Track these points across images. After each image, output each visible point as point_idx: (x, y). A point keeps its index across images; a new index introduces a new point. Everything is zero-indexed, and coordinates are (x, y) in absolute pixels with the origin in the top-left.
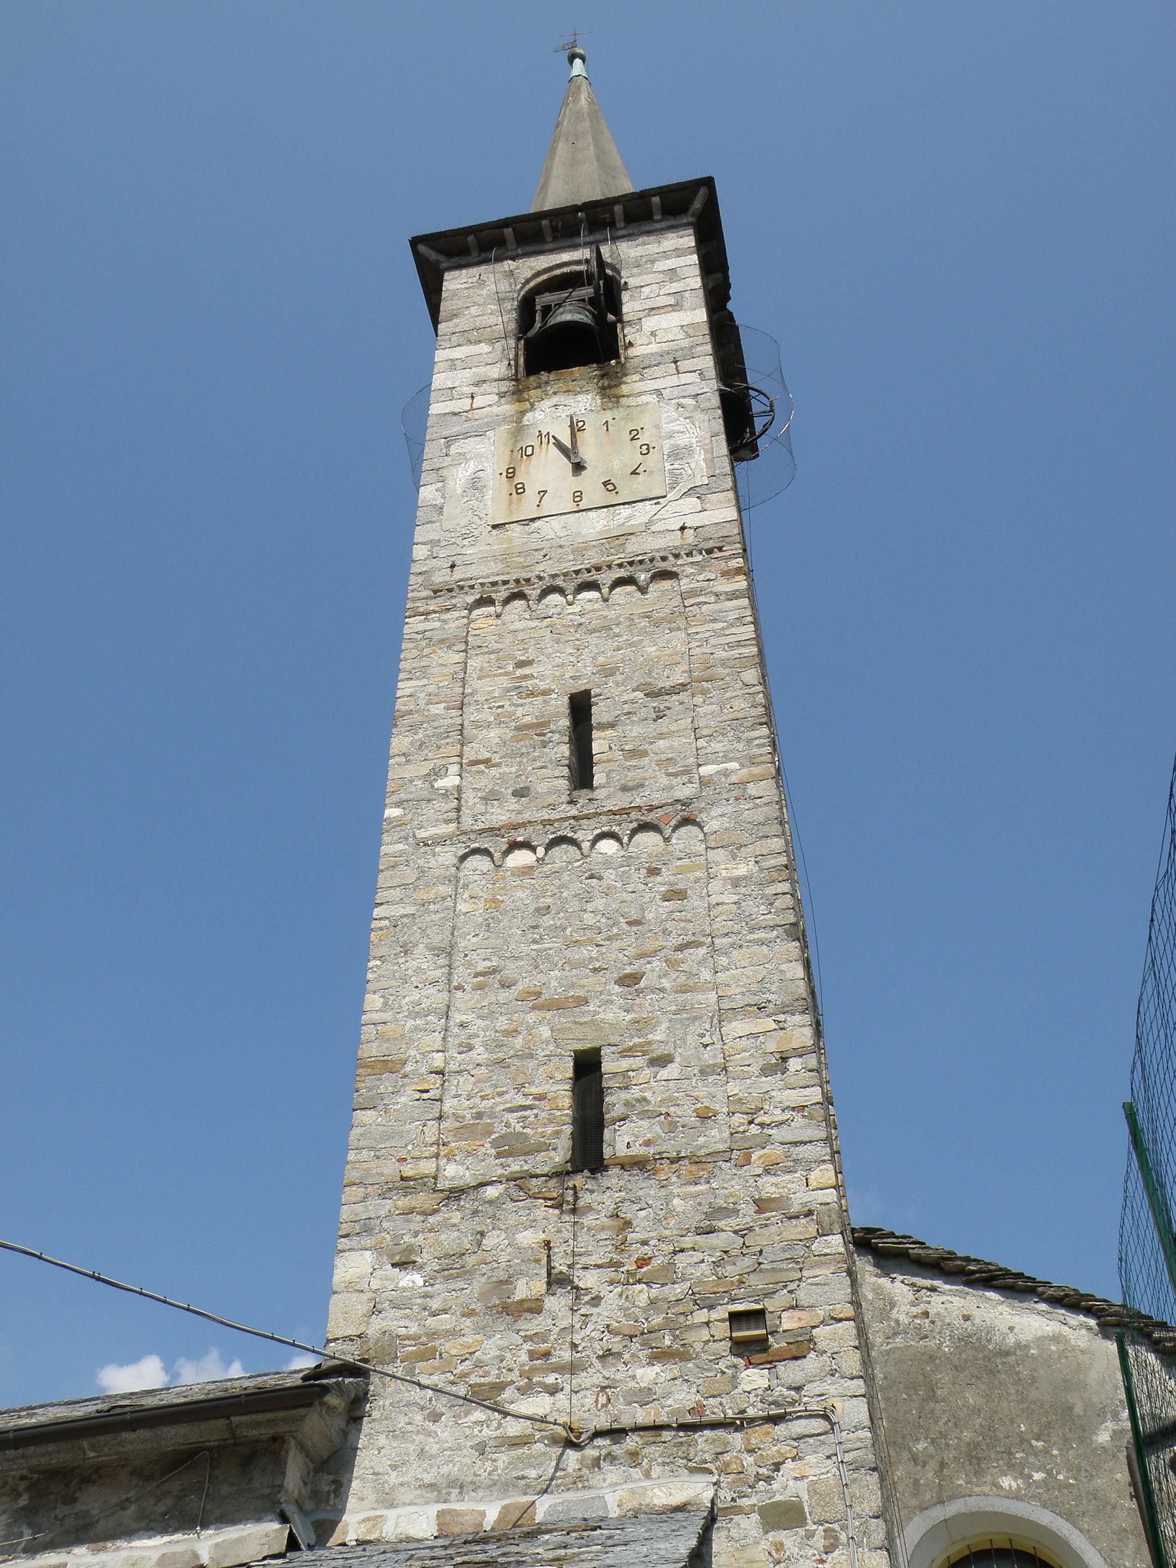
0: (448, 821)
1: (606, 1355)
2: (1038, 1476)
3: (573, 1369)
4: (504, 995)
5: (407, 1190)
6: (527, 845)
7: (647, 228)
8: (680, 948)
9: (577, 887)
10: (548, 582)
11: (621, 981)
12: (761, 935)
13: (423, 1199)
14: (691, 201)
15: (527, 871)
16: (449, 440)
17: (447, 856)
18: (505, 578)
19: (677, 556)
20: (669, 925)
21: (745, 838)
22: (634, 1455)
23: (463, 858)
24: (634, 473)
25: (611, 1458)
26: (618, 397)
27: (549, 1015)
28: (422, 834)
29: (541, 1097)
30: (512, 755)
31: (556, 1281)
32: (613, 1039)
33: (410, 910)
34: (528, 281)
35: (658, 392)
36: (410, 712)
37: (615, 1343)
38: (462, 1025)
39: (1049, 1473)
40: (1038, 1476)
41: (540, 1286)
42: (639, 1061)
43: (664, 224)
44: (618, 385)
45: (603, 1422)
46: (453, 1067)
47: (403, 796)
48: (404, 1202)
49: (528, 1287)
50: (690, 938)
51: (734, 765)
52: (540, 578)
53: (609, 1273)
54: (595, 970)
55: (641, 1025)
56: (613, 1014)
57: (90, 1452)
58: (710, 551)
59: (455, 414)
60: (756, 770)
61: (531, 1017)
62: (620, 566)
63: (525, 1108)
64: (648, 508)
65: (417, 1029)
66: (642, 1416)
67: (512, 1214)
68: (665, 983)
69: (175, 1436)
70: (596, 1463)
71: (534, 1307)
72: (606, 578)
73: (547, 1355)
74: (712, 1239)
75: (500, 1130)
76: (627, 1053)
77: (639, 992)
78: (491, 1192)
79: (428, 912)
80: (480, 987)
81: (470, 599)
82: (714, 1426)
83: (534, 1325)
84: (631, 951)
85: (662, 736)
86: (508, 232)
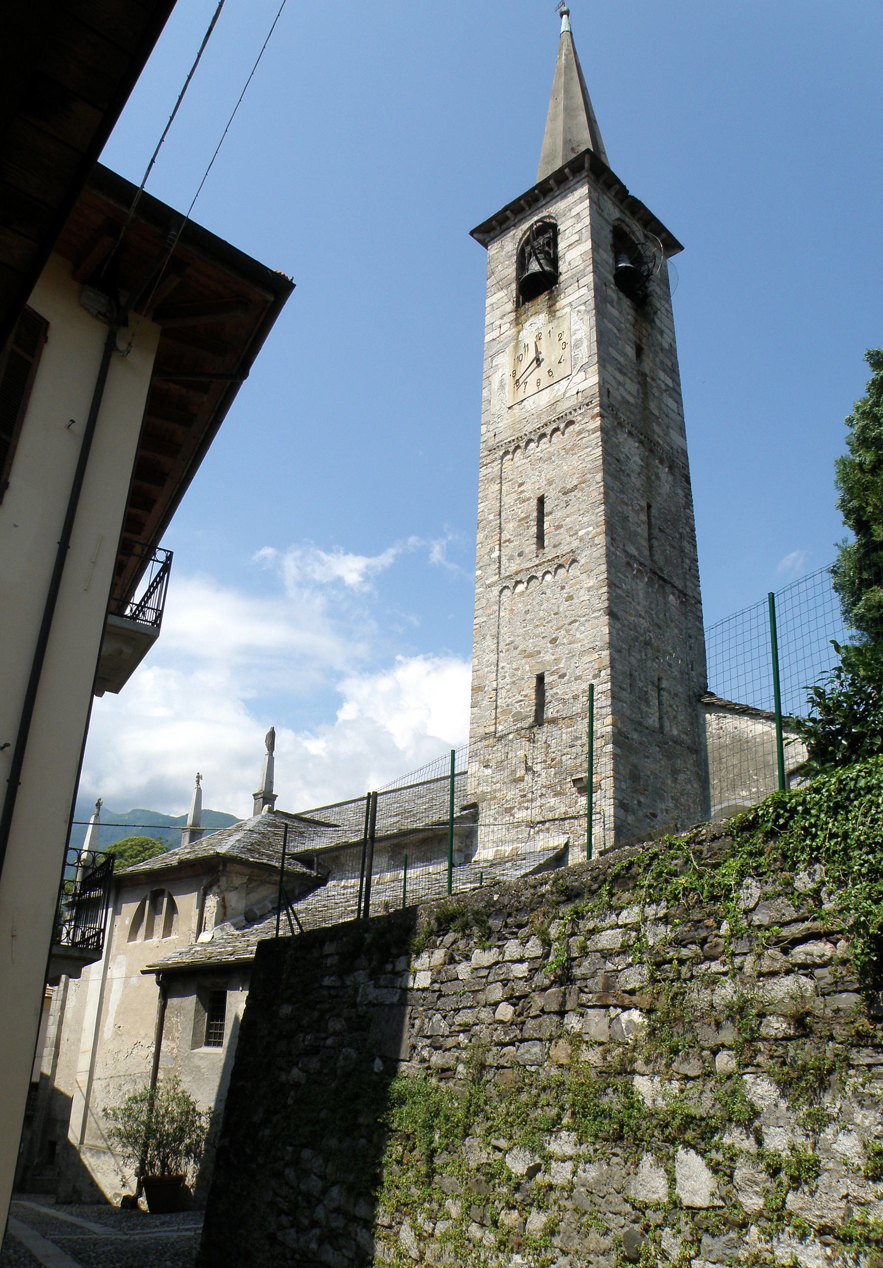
0: (495, 575)
1: (542, 795)
2: (754, 790)
3: (532, 801)
4: (516, 652)
5: (485, 738)
6: (521, 582)
7: (567, 186)
8: (570, 624)
9: (538, 599)
10: (526, 439)
11: (551, 642)
12: (596, 614)
13: (491, 741)
14: (584, 163)
15: (522, 594)
16: (492, 357)
17: (496, 590)
18: (513, 438)
19: (575, 410)
20: (567, 613)
21: (593, 566)
22: (548, 829)
23: (501, 592)
24: (560, 362)
25: (542, 831)
26: (555, 312)
27: (528, 660)
28: (488, 582)
29: (526, 696)
30: (517, 536)
31: (528, 769)
32: (548, 668)
33: (485, 619)
34: (521, 239)
35: (570, 304)
36: (482, 520)
37: (544, 791)
38: (503, 668)
39: (758, 788)
40: (754, 790)
41: (523, 772)
42: (556, 677)
43: (575, 181)
44: (555, 304)
45: (541, 819)
46: (500, 686)
47: (481, 564)
48: (487, 743)
49: (520, 772)
50: (573, 619)
51: (591, 528)
52: (526, 435)
53: (543, 765)
54: (543, 638)
55: (557, 661)
56: (548, 657)
57: (407, 840)
58: (587, 405)
59: (494, 340)
60: (598, 530)
61: (523, 661)
62: (554, 421)
63: (521, 701)
64: (564, 383)
65: (488, 672)
66: (550, 816)
67: (516, 744)
68: (565, 641)
69: (421, 836)
70: (538, 832)
71: (522, 779)
72: (548, 431)
73: (525, 796)
74: (574, 750)
75: (514, 711)
76: (552, 674)
77: (557, 646)
78: (511, 736)
79: (490, 619)
80: (507, 650)
81: (501, 453)
82: (570, 818)
83: (522, 785)
84: (555, 627)
85: (568, 516)
86: (494, 223)
